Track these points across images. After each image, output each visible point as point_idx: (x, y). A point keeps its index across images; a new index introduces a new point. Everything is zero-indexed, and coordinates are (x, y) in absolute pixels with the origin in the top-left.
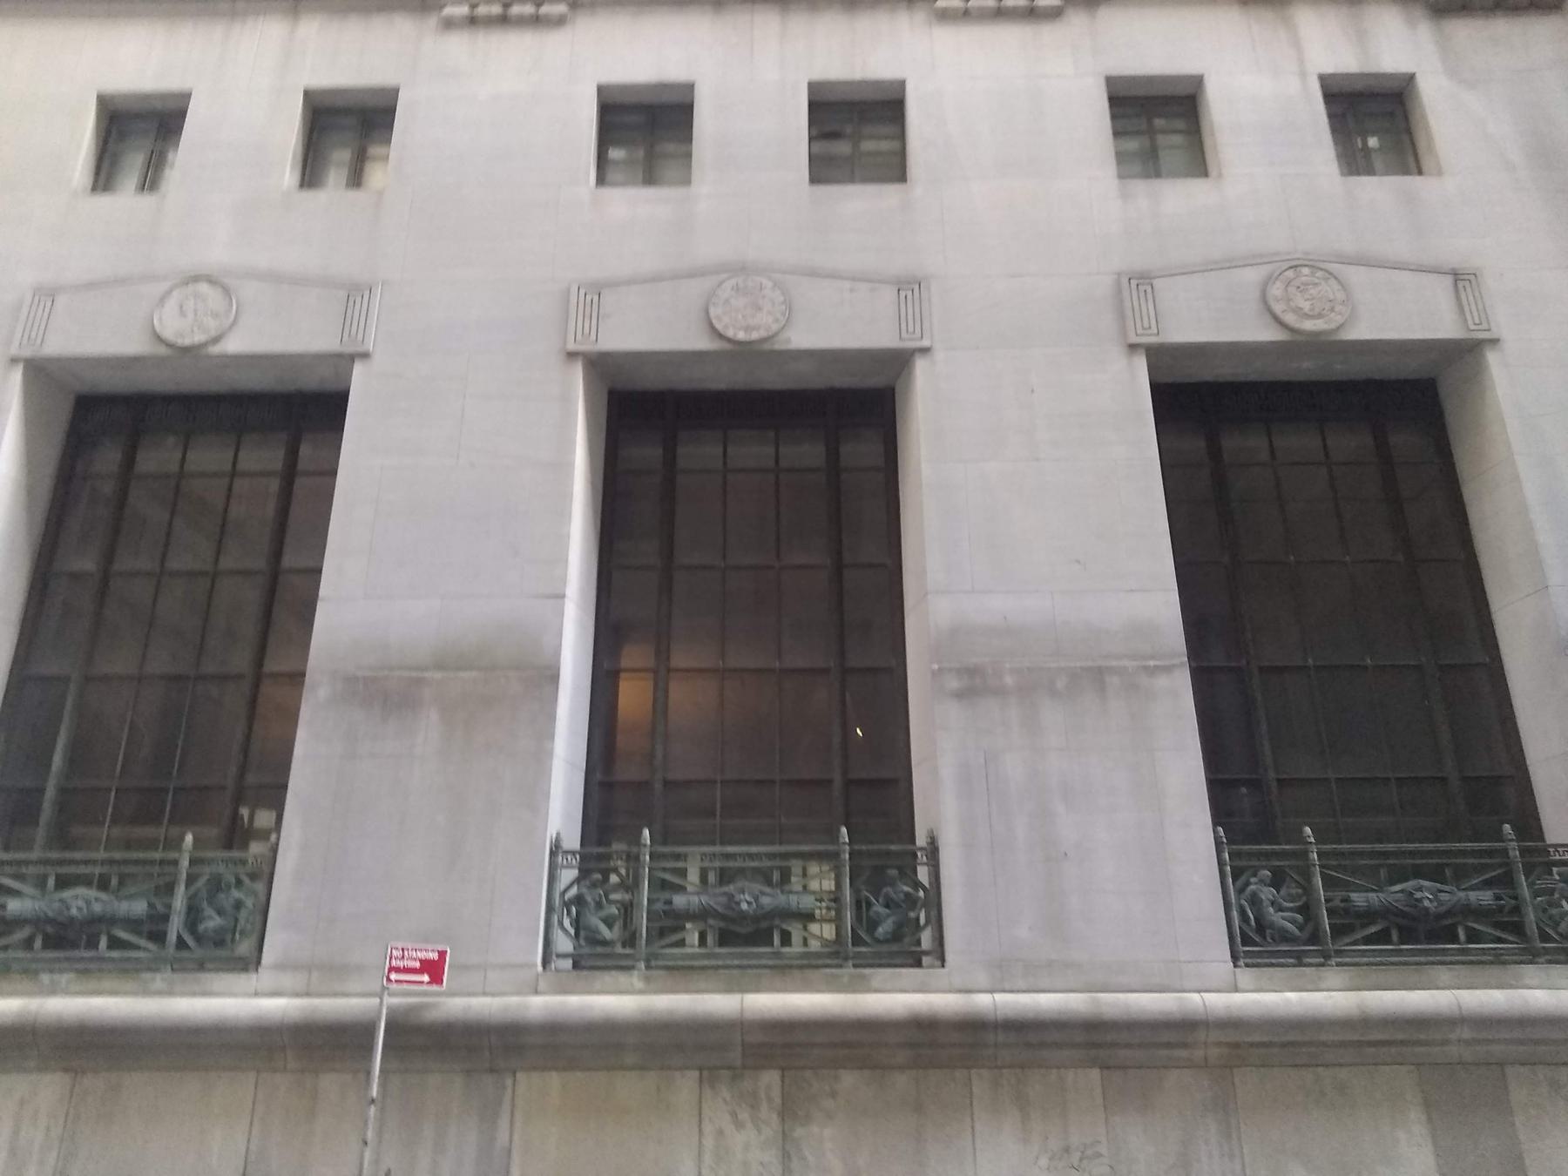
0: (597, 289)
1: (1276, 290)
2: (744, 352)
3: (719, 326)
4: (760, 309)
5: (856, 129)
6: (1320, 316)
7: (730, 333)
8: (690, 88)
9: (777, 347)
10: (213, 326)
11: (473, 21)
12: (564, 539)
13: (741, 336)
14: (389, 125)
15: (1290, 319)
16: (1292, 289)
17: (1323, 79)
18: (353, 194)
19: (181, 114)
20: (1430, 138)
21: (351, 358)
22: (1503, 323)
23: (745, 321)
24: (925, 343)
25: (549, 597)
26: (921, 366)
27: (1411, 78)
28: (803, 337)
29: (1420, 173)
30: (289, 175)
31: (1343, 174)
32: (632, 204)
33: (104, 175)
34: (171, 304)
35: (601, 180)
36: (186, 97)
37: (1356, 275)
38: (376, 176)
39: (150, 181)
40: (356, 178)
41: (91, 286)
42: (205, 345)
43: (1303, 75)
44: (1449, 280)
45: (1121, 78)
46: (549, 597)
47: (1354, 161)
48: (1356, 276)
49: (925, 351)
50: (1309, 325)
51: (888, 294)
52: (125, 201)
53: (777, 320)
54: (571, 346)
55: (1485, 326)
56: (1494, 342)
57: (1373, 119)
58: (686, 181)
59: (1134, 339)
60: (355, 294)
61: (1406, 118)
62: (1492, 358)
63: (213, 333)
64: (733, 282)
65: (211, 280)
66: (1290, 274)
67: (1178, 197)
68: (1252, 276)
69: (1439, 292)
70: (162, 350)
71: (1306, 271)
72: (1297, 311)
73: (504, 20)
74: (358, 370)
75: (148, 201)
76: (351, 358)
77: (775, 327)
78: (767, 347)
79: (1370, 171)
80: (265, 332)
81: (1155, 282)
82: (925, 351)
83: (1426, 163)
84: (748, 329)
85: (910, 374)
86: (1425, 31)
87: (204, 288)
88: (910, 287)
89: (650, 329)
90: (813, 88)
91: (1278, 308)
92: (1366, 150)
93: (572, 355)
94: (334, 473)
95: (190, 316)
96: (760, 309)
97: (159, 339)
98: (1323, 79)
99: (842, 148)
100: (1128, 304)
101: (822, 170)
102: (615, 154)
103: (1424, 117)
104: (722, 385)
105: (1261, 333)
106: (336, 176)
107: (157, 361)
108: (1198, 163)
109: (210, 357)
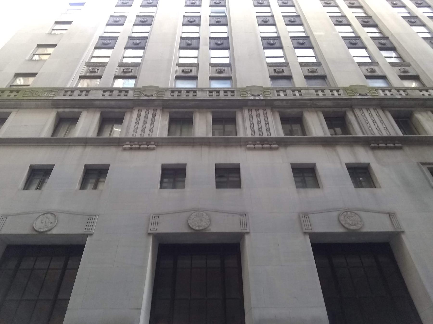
0: (158, 216)
1: (342, 218)
2: (198, 233)
3: (191, 226)
4: (202, 221)
5: (228, 176)
6: (355, 225)
7: (194, 228)
8: (185, 165)
9: (207, 231)
10: (50, 226)
11: (131, 149)
12: (142, 290)
13: (197, 228)
14: (106, 173)
15: (346, 226)
16: (346, 218)
17: (347, 164)
18: (94, 191)
19: (51, 170)
20: (376, 179)
21: (87, 235)
22: (404, 227)
23: (198, 224)
24: (248, 231)
25: (137, 309)
26: (247, 237)
27: (369, 164)
28: (214, 229)
29: (375, 187)
30: (77, 186)
31: (355, 187)
32: (170, 194)
33: (27, 185)
34: (40, 220)
35: (161, 188)
36: (54, 165)
37: (362, 214)
38: (101, 186)
39: (39, 187)
40: (95, 187)
41: (18, 214)
42: (46, 231)
43: (341, 163)
44: (388, 215)
45: (165, 164)
46: (137, 309)
47: (358, 184)
48: (362, 214)
49: (248, 233)
50: (352, 228)
51: (237, 217)
52: (32, 192)
53: (207, 224)
54: (149, 232)
55: (399, 228)
56: (403, 232)
57: (361, 174)
58: (183, 187)
59: (305, 231)
60: (91, 217)
61: (369, 173)
62: (403, 236)
63: (50, 228)
64: (195, 214)
65: (51, 214)
66: (345, 213)
67: (312, 193)
68: (335, 214)
69: (386, 218)
70: (34, 233)
71: (349, 213)
72: (349, 224)
73: (139, 149)
74: (89, 238)
75: (38, 192)
76: (87, 235)
77: (206, 226)
78: (204, 231)
79: (362, 187)
80: (64, 228)
81: (309, 215)
82: (248, 233)
83: (377, 185)
84: (199, 226)
85: (244, 241)
86: (370, 153)
87: (49, 215)
88: (243, 215)
89: (169, 226)
90: (31, 166)
91: (343, 223)
92: (360, 181)
93: (149, 234)
94: (78, 269)
95: (44, 223)
96: (202, 221)
97: (34, 229)
98: (347, 164)
99: (224, 179)
100: (302, 221)
101: (219, 185)
102: (165, 180)
103: (374, 175)
104: (190, 242)
105: (339, 230)
106: (90, 186)
107: (32, 235)
108: (316, 184)
109: (47, 234)
